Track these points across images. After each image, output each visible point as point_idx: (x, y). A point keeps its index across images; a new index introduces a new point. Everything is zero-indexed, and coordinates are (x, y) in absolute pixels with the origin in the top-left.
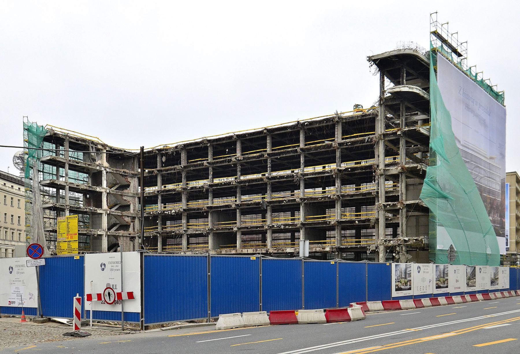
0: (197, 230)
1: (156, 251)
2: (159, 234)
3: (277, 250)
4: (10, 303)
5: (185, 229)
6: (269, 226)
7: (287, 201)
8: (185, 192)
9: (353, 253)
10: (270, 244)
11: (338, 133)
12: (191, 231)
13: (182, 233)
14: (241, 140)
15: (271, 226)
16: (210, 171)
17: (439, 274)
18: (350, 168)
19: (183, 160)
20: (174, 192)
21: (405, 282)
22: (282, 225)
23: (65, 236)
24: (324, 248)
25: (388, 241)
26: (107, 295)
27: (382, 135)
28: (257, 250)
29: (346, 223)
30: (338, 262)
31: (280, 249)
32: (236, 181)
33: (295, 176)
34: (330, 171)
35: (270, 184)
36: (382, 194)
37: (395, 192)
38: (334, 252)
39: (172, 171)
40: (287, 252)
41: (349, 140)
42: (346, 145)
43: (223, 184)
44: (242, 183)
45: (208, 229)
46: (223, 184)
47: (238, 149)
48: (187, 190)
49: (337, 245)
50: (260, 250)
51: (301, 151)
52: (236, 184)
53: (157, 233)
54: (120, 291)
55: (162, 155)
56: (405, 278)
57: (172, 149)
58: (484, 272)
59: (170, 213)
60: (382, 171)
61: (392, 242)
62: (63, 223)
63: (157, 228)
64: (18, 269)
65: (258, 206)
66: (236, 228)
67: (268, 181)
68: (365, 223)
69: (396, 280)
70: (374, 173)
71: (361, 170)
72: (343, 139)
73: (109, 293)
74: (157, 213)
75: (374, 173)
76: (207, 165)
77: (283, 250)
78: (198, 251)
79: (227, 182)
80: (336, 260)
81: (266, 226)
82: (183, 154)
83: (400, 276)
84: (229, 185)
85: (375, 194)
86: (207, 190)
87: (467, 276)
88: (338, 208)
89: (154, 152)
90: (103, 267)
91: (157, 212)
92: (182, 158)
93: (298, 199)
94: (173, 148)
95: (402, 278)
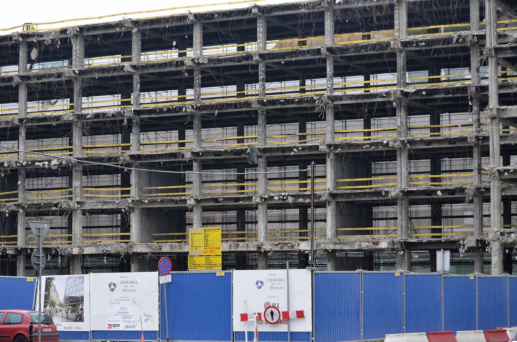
0: (105, 203)
1: (11, 243)
2: (23, 208)
3: (279, 246)
4: (110, 326)
5: (78, 199)
6: (262, 198)
7: (300, 148)
8: (79, 123)
9: (427, 251)
10: (263, 234)
11: (400, 23)
12: (91, 204)
13: (74, 208)
14: (202, 24)
15: (267, 197)
16: (135, 82)
18: (424, 90)
19: (76, 57)
20: (56, 123)
22: (289, 195)
23: (202, 249)
24: (377, 244)
25: (507, 233)
26: (270, 314)
27: (493, 50)
28: (238, 244)
29: (419, 195)
30: (478, 276)
31: (287, 244)
32: (193, 106)
33: (317, 101)
34: (386, 94)
35: (265, 113)
36: (495, 151)
37: (509, 137)
38: (398, 250)
39: (52, 79)
40: (300, 250)
41: (421, 37)
42: (416, 47)
43: (165, 110)
44: (204, 110)
45: (133, 201)
46: (165, 110)
47: (196, 42)
48: (85, 119)
49: (400, 237)
50: (245, 245)
51: (327, 53)
52: (193, 111)
53: (18, 206)
54: (286, 310)
55: (30, 46)
57: (53, 34)
59: (46, 166)
60: (494, 111)
61: (513, 235)
62: (198, 235)
63: (16, 196)
65: (238, 157)
66: (193, 200)
67: (261, 107)
68: (454, 194)
70: (470, 102)
71: (445, 94)
72: (409, 34)
73: (272, 313)
74: (18, 164)
75: (470, 102)
76: (132, 70)
77: (292, 246)
78: (110, 245)
79: (174, 107)
80: (475, 274)
81: (257, 197)
82: (76, 45)
84: (176, 112)
85: (474, 141)
86: (130, 120)
88: (403, 165)
89: (15, 40)
90: (112, 287)
91: (19, 162)
92: (74, 53)
93: (324, 145)
94: (55, 32)
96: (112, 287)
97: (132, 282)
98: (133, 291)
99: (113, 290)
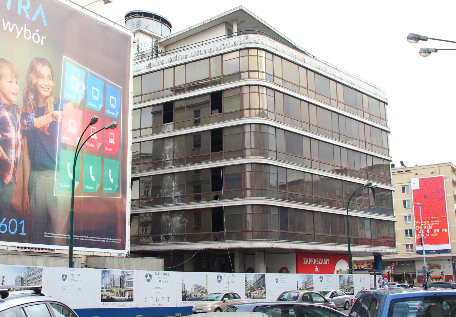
17: (343, 282)
21: (348, 289)
56: (348, 285)
58: (363, 281)
64: (228, 279)
69: (340, 287)
83: (343, 284)
87: (246, 286)
90: (64, 277)
95: (345, 285)
96: (64, 277)
97: (78, 275)
98: (166, 282)
99: (64, 280)
